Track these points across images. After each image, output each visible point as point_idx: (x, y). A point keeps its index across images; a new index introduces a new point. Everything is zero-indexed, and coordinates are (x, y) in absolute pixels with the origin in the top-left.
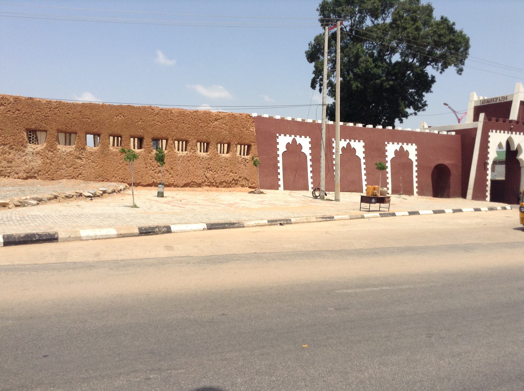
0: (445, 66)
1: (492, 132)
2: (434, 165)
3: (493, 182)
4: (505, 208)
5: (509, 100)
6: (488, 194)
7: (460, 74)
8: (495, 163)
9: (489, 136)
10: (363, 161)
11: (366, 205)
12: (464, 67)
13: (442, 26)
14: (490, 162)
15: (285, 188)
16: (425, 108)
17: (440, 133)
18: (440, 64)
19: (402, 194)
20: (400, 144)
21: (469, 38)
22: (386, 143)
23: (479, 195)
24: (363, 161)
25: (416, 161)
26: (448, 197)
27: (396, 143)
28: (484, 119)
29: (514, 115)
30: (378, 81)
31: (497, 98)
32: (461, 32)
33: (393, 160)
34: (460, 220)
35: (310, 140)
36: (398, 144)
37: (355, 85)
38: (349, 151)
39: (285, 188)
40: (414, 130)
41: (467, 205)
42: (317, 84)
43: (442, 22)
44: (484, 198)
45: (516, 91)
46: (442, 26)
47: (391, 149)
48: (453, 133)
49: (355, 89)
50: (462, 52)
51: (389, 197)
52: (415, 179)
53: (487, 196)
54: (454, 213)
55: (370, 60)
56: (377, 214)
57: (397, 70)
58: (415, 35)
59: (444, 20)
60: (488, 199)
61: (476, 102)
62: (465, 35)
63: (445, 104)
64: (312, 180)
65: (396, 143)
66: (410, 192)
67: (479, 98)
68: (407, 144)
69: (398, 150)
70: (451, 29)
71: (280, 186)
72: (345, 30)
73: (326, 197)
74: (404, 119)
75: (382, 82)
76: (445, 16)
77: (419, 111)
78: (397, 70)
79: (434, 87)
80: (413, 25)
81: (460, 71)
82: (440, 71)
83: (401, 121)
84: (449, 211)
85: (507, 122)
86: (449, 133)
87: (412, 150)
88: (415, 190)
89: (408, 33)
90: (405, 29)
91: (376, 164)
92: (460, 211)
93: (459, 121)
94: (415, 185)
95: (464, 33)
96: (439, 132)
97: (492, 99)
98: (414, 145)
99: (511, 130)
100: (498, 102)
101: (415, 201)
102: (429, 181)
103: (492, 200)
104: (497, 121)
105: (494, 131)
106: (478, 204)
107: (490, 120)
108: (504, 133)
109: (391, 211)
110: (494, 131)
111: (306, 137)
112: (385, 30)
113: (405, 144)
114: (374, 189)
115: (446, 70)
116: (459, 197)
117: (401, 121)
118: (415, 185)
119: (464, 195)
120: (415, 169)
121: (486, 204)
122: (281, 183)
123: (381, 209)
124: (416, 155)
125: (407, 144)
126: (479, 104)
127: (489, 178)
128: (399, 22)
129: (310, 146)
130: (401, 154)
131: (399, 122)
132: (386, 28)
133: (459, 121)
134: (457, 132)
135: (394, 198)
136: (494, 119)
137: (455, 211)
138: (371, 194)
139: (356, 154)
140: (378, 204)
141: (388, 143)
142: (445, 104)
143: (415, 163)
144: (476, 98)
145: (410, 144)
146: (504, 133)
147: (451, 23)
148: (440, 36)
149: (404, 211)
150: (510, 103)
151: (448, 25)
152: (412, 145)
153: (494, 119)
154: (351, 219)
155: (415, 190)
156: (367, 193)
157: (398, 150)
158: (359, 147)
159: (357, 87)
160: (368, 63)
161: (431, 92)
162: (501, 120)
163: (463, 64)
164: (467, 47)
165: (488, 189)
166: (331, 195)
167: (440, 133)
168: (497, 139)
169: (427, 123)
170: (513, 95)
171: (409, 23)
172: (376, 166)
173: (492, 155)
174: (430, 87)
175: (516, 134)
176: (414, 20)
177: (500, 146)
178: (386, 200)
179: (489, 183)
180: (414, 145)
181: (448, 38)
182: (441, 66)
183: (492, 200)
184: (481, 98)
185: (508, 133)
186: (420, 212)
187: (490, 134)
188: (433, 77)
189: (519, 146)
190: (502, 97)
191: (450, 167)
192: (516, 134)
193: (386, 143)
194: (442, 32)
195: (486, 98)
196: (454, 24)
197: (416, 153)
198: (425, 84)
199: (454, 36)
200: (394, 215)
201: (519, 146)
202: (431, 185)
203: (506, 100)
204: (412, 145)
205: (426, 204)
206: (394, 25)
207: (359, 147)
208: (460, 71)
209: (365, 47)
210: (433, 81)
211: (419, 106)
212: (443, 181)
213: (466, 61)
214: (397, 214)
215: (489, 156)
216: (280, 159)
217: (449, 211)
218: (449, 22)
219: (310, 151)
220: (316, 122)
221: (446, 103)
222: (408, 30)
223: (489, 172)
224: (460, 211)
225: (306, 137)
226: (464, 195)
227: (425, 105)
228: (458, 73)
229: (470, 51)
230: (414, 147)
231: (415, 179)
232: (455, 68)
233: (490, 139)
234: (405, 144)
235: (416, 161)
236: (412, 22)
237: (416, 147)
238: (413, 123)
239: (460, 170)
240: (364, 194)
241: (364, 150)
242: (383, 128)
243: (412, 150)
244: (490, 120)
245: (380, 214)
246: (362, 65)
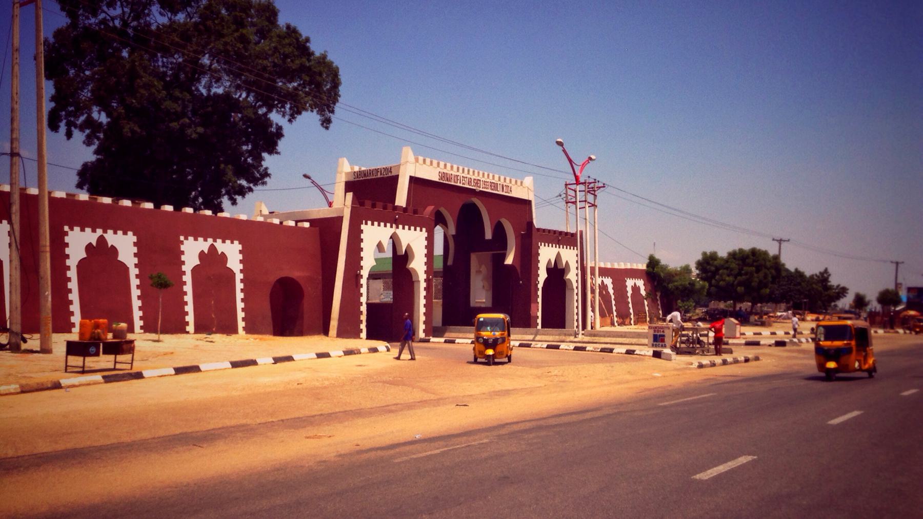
0: (296, 111)
1: (366, 224)
2: (273, 279)
3: (370, 306)
4: (374, 350)
5: (394, 174)
6: (363, 326)
7: (327, 128)
8: (373, 276)
9: (362, 231)
10: (134, 272)
11: (75, 361)
12: (333, 117)
13: (287, 41)
14: (365, 273)
15: (198, 330)
16: (267, 179)
17: (285, 223)
18: (288, 106)
19: (216, 333)
20: (99, 232)
21: (338, 68)
22: (182, 238)
23: (348, 330)
24: (134, 272)
25: (241, 271)
26: (301, 333)
27: (88, 230)
28: (353, 203)
29: (401, 199)
30: (174, 125)
31: (377, 170)
32: (324, 57)
33: (195, 270)
34: (284, 375)
35: (240, 247)
36: (205, 240)
37: (128, 128)
38: (101, 254)
39: (198, 330)
40: (236, 216)
41: (334, 344)
42: (61, 121)
43: (288, 34)
44: (356, 334)
45: (402, 161)
46: (287, 41)
47: (192, 250)
48: (307, 225)
49: (129, 134)
50: (329, 91)
51: (132, 342)
52: (240, 305)
53: (361, 331)
54: (275, 363)
55: (158, 84)
56: (98, 377)
57: (210, 109)
58: (239, 48)
59: (292, 32)
60: (364, 335)
61: (347, 174)
62: (332, 63)
63: (306, 176)
64: (141, 313)
65: (88, 230)
66: (229, 328)
67: (352, 168)
68: (224, 242)
69: (206, 252)
70: (302, 48)
71: (73, 325)
72: (111, 24)
73: (24, 346)
74: (239, 198)
75: (183, 127)
76: (293, 24)
77: (255, 184)
78: (210, 109)
79: (282, 145)
80: (237, 30)
81: (326, 123)
82: (287, 117)
83: (234, 202)
84: (265, 360)
85: (390, 210)
86: (300, 224)
87: (232, 253)
88: (241, 324)
89: (226, 44)
90: (220, 35)
91: (151, 278)
92: (289, 359)
93: (330, 204)
94: (241, 315)
95: (330, 57)
96: (281, 223)
97: (371, 172)
98: (236, 242)
99: (395, 222)
100: (379, 176)
101: (242, 343)
102: (265, 307)
103: (370, 337)
104: (374, 206)
105: (369, 223)
106: (351, 343)
107: (362, 204)
108: (409, 229)
109: (137, 366)
110: (369, 223)
111: (125, 233)
112: (185, 33)
113: (219, 241)
114: (97, 326)
115: (299, 117)
116: (319, 333)
117: (234, 202)
118: (241, 315)
119: (325, 331)
120: (239, 286)
121: (363, 343)
122: (190, 318)
123: (118, 366)
124: (241, 261)
125: (224, 242)
126: (351, 179)
127: (363, 299)
128: (209, 23)
129: (241, 257)
130: (212, 259)
131: (229, 203)
132: (188, 30)
133: (330, 204)
134: (313, 222)
135: (142, 341)
136: (368, 203)
137: (277, 360)
138: (88, 336)
139: (198, 262)
140: (112, 357)
141: (186, 238)
142: (306, 176)
143: (239, 276)
144: (346, 168)
145: (228, 242)
146: (385, 226)
147: (304, 37)
148: (286, 56)
149: (166, 367)
150: (396, 178)
151: (297, 39)
152: (232, 243)
153: (368, 203)
154: (23, 392)
155: (241, 324)
156: (81, 334)
157: (206, 252)
158: (125, 245)
159: (132, 131)
160: (153, 90)
161: (278, 153)
162: (380, 205)
163: (333, 112)
164: (336, 84)
165: (363, 318)
166: (34, 342)
167: (285, 223)
168: (375, 235)
169: (266, 206)
170: (399, 166)
171: (229, 27)
172: (151, 282)
173: (368, 262)
174: (276, 144)
175: (404, 228)
176: (240, 24)
177: (380, 247)
178: (125, 347)
179: (364, 308)
180: (236, 242)
181: (297, 62)
182: (291, 109)
183: (370, 337)
184: (356, 169)
185: (391, 227)
186: (202, 367)
187: (363, 227)
188: (279, 128)
189: (409, 246)
190: (385, 169)
191: (302, 283)
192: (404, 228)
193: (182, 238)
194: (288, 50)
195: (363, 169)
196: (308, 40)
197: (135, 250)
198: (269, 140)
199: (309, 60)
200: (139, 376)
201: (409, 246)
202: (269, 314)
203: (390, 175)
204: (232, 243)
205: (265, 348)
206: (201, 27)
207: (125, 245)
208: (326, 123)
209: (160, 64)
210: (279, 134)
211: (258, 177)
212: (290, 309)
213: (338, 108)
214: (145, 374)
215: (362, 263)
216: (188, 278)
217: (265, 360)
218: (300, 35)
219: (136, 260)
220: (76, 198)
221: (308, 174)
222: (228, 39)
223: (363, 290)
224: (289, 359)
225: (125, 233)
226: (325, 331)
227: (266, 174)
228: (322, 125)
229: (342, 89)
230: (237, 246)
231: (240, 305)
232: (319, 117)
233: (362, 236)
234: (219, 241)
235: (241, 271)
236: (233, 27)
237: (240, 247)
238: (253, 207)
239: (320, 286)
240: (74, 336)
241: (135, 250)
242: (155, 207)
243: (232, 253)
244: (362, 204)
245: (104, 377)
246: (142, 91)
